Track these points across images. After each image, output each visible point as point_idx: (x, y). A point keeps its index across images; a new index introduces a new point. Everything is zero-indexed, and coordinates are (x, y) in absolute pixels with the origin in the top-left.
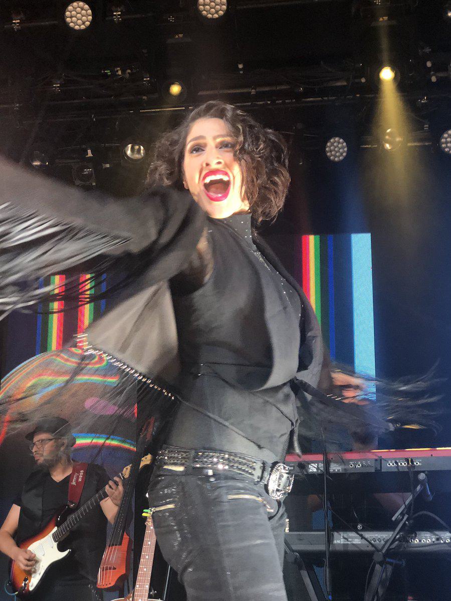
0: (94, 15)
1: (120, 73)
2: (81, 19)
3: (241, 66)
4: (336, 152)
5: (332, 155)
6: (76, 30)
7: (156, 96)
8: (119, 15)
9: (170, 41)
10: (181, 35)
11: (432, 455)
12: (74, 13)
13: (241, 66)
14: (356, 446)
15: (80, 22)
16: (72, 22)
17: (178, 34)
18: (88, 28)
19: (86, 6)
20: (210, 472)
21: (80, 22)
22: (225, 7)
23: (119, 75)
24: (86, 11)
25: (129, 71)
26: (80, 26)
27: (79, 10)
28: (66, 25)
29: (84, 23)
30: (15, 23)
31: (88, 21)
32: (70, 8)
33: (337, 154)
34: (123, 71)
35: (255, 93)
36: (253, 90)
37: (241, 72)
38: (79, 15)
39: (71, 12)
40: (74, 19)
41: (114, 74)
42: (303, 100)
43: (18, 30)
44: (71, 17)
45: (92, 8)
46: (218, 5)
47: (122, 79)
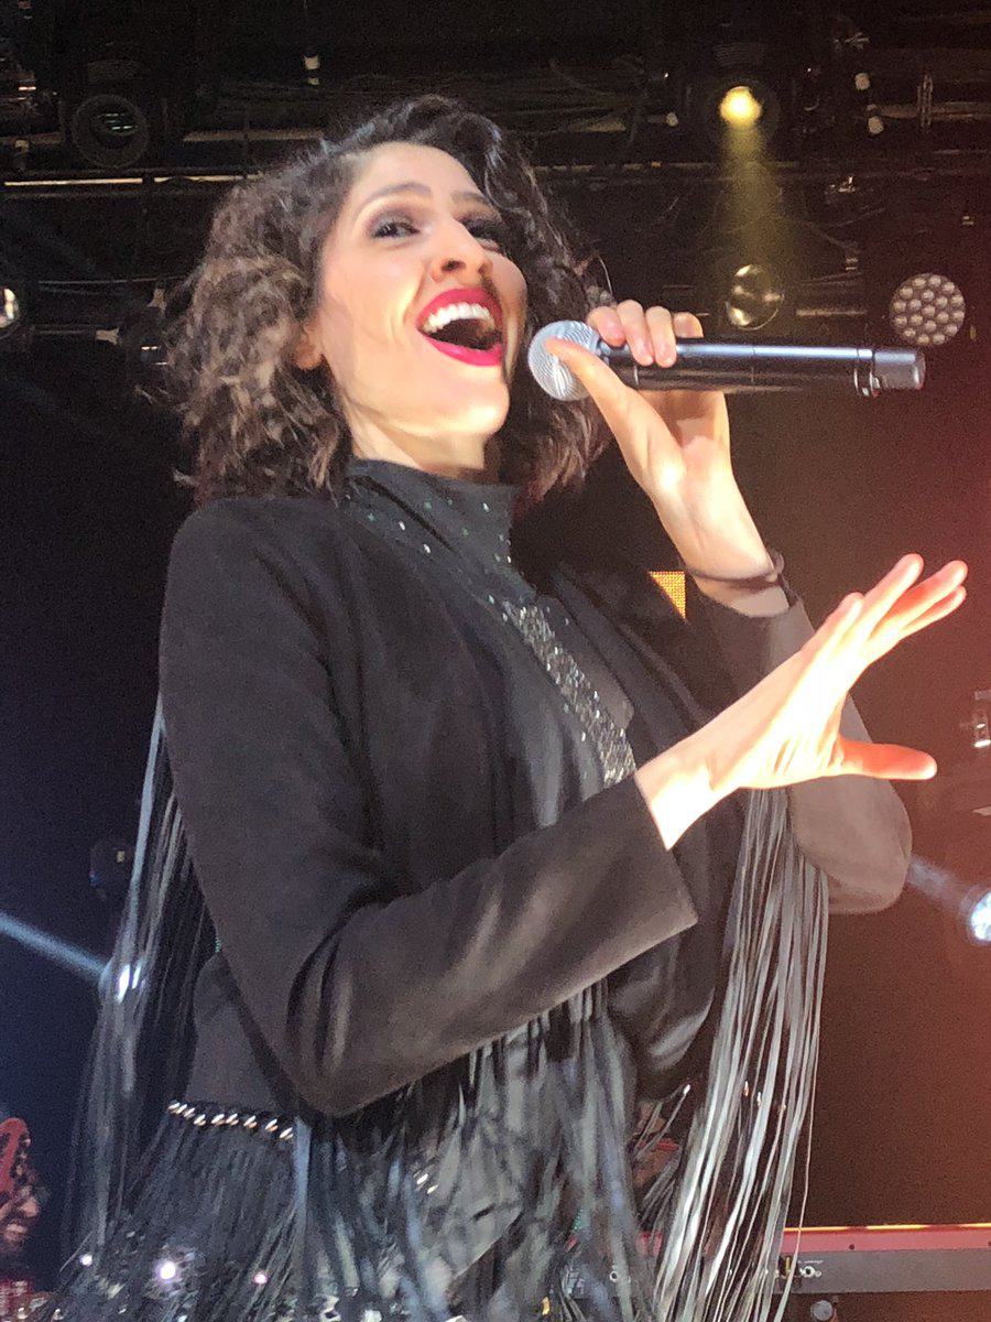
3: (312, 63)
21: (931, 325)
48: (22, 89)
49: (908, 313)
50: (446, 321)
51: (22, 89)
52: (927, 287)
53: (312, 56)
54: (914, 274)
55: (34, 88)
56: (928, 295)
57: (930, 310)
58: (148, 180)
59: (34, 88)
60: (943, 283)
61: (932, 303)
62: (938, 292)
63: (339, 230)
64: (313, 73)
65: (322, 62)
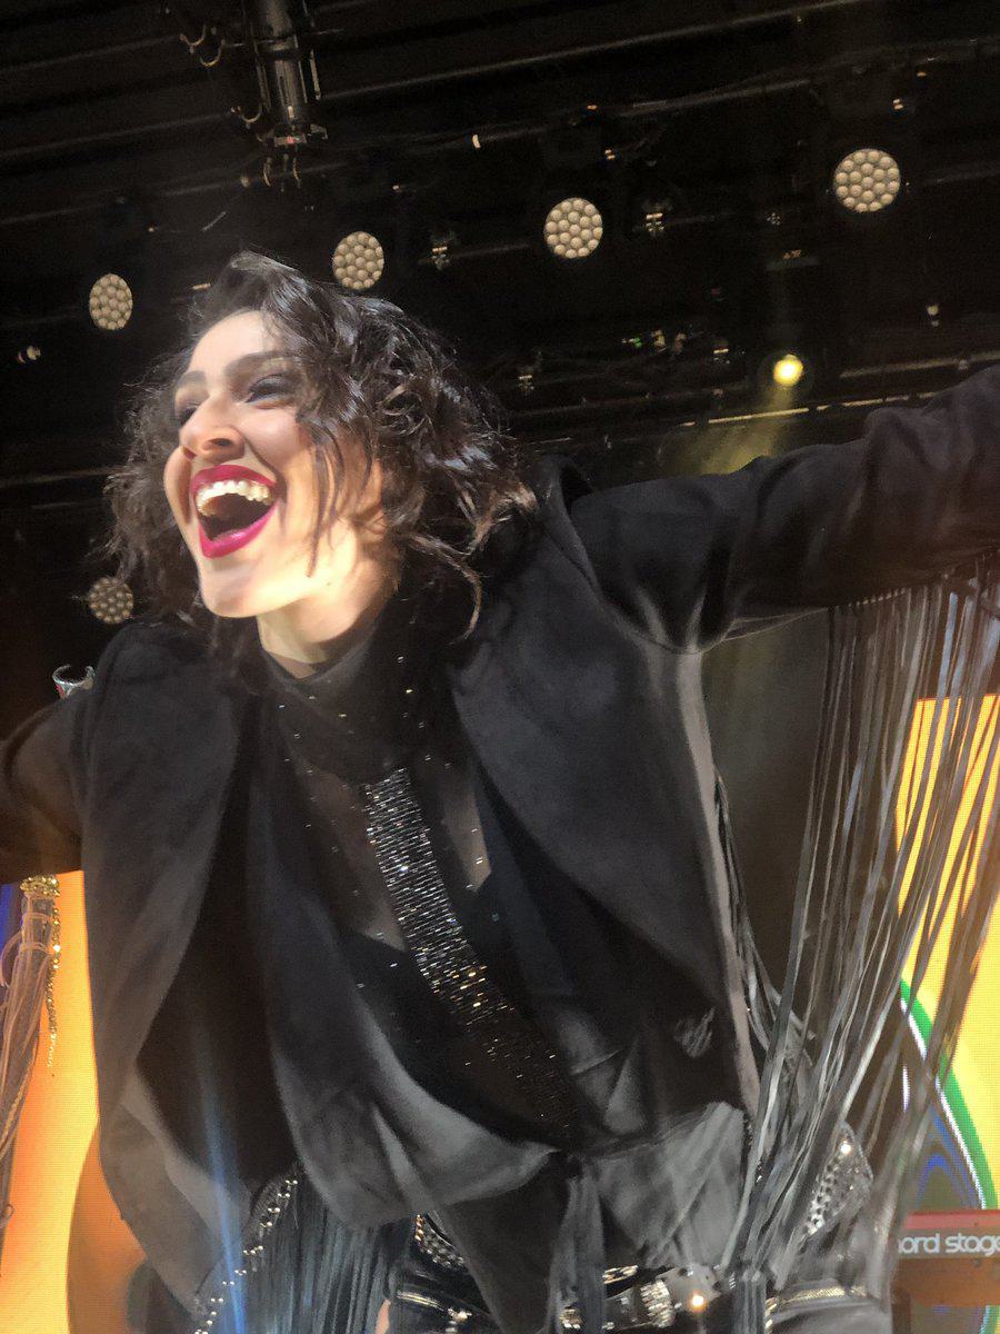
0: (606, 224)
1: (661, 341)
2: (364, 269)
3: (932, 311)
4: (110, 605)
5: (99, 609)
6: (570, 261)
7: (737, 387)
8: (658, 220)
9: (773, 266)
10: (796, 253)
11: (976, 1224)
12: (563, 223)
13: (932, 311)
14: (657, 1181)
15: (576, 241)
16: (559, 243)
17: (789, 249)
18: (594, 254)
19: (590, 208)
20: (288, 1195)
21: (576, 241)
22: (131, 303)
23: (660, 348)
24: (886, 169)
25: (681, 336)
26: (577, 250)
27: (573, 215)
28: (547, 250)
29: (585, 243)
30: (437, 254)
31: (593, 238)
32: (847, 163)
33: (112, 610)
34: (670, 339)
35: (966, 367)
36: (963, 362)
37: (935, 323)
38: (868, 180)
39: (557, 222)
40: (564, 236)
41: (648, 343)
42: (34, 507)
43: (445, 268)
44: (558, 232)
45: (601, 209)
46: (853, 171)
47: (667, 354)
48: (716, 352)
49: (848, 184)
50: (222, 493)
51: (716, 352)
52: (867, 161)
53: (932, 305)
54: (841, 157)
55: (726, 350)
56: (867, 167)
57: (359, 261)
58: (813, 409)
59: (726, 350)
60: (881, 157)
61: (362, 255)
62: (876, 165)
63: (245, 315)
64: (935, 318)
65: (941, 306)
